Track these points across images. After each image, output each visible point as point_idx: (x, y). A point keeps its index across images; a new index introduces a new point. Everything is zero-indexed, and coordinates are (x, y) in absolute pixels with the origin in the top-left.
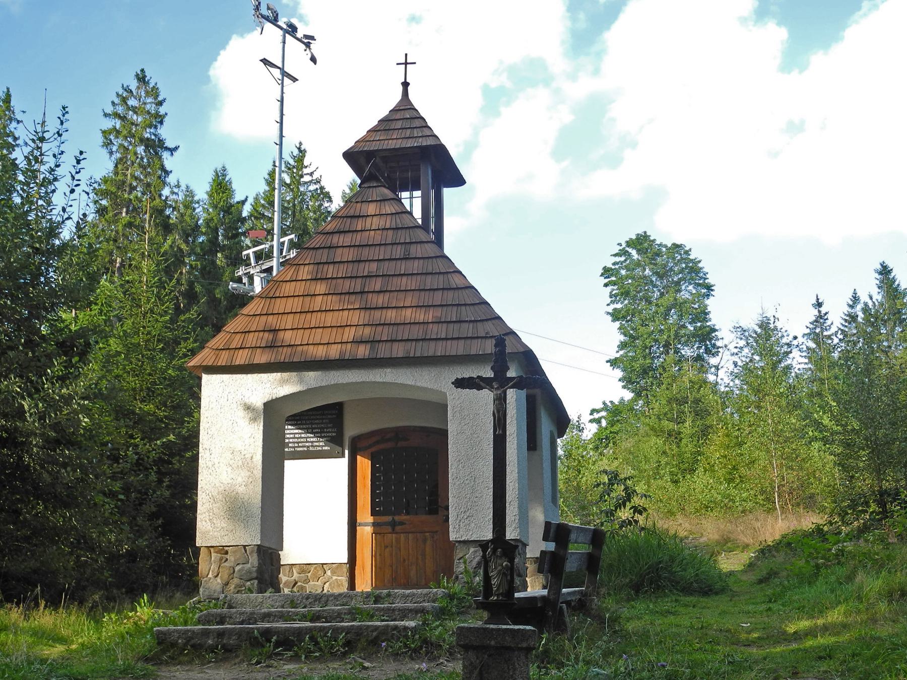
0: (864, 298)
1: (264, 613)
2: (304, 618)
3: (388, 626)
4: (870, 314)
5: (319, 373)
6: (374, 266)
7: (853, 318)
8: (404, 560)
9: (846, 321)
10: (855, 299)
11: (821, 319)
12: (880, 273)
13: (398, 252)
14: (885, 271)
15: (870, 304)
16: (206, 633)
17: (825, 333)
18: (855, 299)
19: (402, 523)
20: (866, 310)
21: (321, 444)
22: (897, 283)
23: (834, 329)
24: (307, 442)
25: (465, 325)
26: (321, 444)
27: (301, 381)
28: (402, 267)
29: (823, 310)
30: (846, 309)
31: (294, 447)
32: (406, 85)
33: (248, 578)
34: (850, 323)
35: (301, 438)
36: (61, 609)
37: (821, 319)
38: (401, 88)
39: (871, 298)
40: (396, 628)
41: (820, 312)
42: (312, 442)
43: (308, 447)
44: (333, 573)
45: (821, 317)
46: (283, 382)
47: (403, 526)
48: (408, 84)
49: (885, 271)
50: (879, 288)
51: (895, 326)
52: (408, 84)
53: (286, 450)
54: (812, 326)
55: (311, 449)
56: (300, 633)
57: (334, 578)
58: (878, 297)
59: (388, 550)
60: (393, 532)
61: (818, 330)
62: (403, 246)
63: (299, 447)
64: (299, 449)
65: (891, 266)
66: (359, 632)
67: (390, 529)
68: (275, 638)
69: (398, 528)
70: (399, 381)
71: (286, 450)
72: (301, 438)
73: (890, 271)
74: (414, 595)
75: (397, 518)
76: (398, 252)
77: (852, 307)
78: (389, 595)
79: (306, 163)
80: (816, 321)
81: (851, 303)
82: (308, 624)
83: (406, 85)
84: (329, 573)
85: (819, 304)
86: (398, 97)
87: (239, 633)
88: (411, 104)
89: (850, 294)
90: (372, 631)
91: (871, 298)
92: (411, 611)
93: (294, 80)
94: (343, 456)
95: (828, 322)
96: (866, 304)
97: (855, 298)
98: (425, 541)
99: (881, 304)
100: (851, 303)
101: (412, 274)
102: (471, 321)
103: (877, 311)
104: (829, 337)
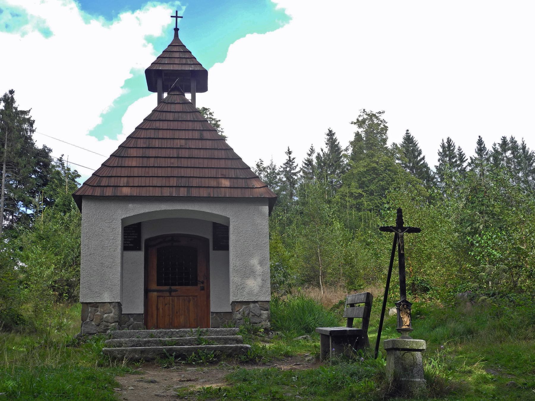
0: (318, 150)
1: (146, 341)
2: (218, 340)
3: (237, 347)
4: (321, 161)
6: (183, 142)
7: (309, 162)
8: (177, 313)
9: (306, 164)
10: (312, 151)
11: (290, 162)
12: (328, 135)
13: (196, 135)
14: (331, 134)
15: (321, 154)
16: (135, 351)
17: (292, 171)
18: (312, 151)
19: (176, 291)
20: (318, 157)
22: (337, 142)
23: (298, 169)
25: (240, 180)
28: (200, 144)
29: (292, 156)
30: (307, 157)
32: (176, 30)
33: (113, 321)
34: (308, 166)
37: (290, 162)
38: (173, 32)
39: (322, 150)
40: (242, 347)
41: (290, 157)
44: (134, 319)
45: (290, 160)
47: (177, 293)
48: (178, 29)
49: (331, 134)
50: (326, 144)
51: (336, 168)
52: (178, 29)
54: (284, 166)
56: (188, 350)
57: (135, 322)
58: (326, 150)
59: (167, 306)
60: (170, 296)
61: (288, 169)
62: (199, 132)
66: (222, 349)
67: (168, 294)
68: (174, 353)
69: (173, 294)
73: (334, 134)
74: (222, 331)
75: (173, 288)
76: (196, 135)
77: (310, 155)
78: (207, 331)
80: (287, 163)
81: (310, 153)
83: (176, 30)
84: (132, 319)
85: (290, 153)
86: (172, 38)
87: (154, 351)
88: (180, 42)
89: (309, 147)
90: (229, 349)
91: (322, 150)
92: (230, 339)
94: (139, 249)
95: (295, 164)
96: (319, 154)
97: (312, 149)
98: (189, 301)
99: (328, 155)
100: (310, 153)
101: (206, 149)
102: (243, 178)
103: (325, 159)
104: (295, 174)
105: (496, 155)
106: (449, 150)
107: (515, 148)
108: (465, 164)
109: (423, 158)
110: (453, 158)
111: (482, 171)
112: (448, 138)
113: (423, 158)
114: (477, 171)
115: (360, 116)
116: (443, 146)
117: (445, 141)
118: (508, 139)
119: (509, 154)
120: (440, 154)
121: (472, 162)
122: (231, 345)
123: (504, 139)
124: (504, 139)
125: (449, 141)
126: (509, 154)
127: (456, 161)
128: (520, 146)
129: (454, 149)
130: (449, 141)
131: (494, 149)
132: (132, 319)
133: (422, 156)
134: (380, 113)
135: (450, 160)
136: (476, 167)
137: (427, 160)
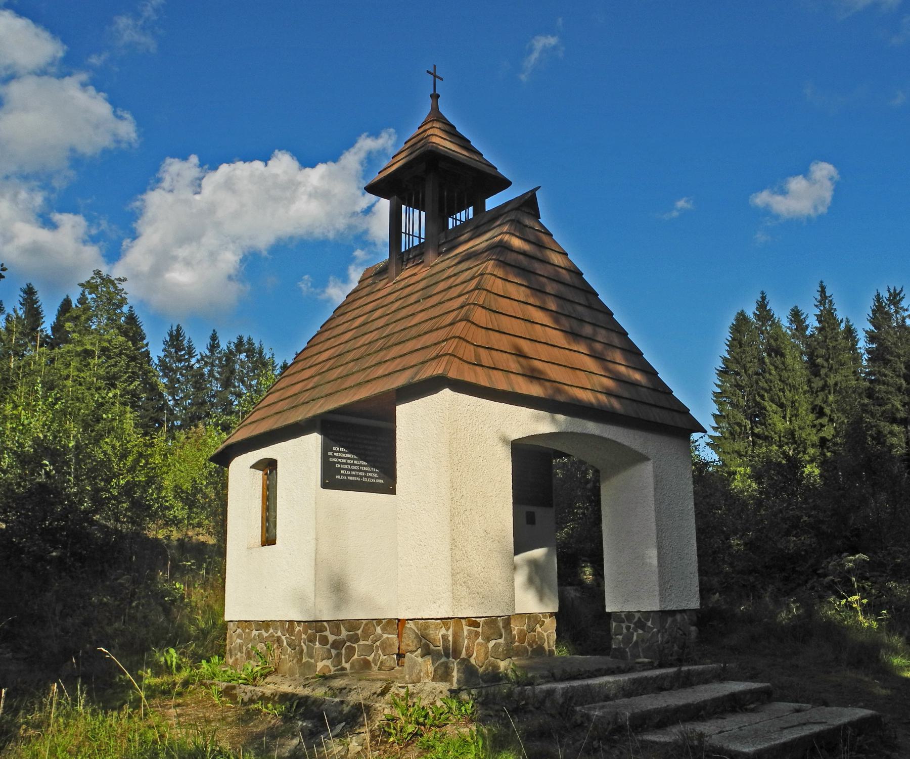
5: (569, 418)
12: (25, 293)
21: (375, 475)
22: (39, 304)
24: (360, 471)
26: (375, 475)
27: (554, 420)
31: (346, 475)
35: (353, 464)
36: (455, 739)
42: (366, 472)
43: (361, 477)
44: (384, 630)
46: (538, 419)
48: (438, 96)
50: (21, 304)
53: (338, 477)
55: (365, 480)
57: (385, 636)
63: (351, 475)
64: (351, 478)
65: (36, 289)
70: (605, 435)
71: (338, 477)
72: (353, 464)
79: (827, 295)
82: (658, 672)
93: (442, 79)
105: (230, 356)
106: (178, 340)
107: (250, 352)
108: (193, 361)
109: (147, 345)
110: (181, 350)
111: (211, 371)
112: (178, 326)
113: (147, 345)
114: (206, 371)
115: (93, 278)
116: (171, 335)
117: (175, 328)
118: (245, 340)
119: (243, 356)
120: (165, 342)
121: (202, 359)
122: (696, 667)
123: (240, 339)
124: (240, 339)
125: (179, 329)
126: (243, 356)
127: (184, 355)
128: (257, 350)
129: (184, 339)
130: (179, 329)
131: (228, 348)
132: (379, 630)
133: (145, 342)
134: (120, 279)
135: (176, 352)
136: (206, 364)
137: (150, 348)
